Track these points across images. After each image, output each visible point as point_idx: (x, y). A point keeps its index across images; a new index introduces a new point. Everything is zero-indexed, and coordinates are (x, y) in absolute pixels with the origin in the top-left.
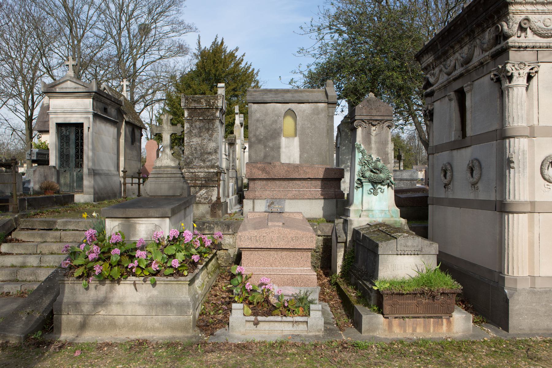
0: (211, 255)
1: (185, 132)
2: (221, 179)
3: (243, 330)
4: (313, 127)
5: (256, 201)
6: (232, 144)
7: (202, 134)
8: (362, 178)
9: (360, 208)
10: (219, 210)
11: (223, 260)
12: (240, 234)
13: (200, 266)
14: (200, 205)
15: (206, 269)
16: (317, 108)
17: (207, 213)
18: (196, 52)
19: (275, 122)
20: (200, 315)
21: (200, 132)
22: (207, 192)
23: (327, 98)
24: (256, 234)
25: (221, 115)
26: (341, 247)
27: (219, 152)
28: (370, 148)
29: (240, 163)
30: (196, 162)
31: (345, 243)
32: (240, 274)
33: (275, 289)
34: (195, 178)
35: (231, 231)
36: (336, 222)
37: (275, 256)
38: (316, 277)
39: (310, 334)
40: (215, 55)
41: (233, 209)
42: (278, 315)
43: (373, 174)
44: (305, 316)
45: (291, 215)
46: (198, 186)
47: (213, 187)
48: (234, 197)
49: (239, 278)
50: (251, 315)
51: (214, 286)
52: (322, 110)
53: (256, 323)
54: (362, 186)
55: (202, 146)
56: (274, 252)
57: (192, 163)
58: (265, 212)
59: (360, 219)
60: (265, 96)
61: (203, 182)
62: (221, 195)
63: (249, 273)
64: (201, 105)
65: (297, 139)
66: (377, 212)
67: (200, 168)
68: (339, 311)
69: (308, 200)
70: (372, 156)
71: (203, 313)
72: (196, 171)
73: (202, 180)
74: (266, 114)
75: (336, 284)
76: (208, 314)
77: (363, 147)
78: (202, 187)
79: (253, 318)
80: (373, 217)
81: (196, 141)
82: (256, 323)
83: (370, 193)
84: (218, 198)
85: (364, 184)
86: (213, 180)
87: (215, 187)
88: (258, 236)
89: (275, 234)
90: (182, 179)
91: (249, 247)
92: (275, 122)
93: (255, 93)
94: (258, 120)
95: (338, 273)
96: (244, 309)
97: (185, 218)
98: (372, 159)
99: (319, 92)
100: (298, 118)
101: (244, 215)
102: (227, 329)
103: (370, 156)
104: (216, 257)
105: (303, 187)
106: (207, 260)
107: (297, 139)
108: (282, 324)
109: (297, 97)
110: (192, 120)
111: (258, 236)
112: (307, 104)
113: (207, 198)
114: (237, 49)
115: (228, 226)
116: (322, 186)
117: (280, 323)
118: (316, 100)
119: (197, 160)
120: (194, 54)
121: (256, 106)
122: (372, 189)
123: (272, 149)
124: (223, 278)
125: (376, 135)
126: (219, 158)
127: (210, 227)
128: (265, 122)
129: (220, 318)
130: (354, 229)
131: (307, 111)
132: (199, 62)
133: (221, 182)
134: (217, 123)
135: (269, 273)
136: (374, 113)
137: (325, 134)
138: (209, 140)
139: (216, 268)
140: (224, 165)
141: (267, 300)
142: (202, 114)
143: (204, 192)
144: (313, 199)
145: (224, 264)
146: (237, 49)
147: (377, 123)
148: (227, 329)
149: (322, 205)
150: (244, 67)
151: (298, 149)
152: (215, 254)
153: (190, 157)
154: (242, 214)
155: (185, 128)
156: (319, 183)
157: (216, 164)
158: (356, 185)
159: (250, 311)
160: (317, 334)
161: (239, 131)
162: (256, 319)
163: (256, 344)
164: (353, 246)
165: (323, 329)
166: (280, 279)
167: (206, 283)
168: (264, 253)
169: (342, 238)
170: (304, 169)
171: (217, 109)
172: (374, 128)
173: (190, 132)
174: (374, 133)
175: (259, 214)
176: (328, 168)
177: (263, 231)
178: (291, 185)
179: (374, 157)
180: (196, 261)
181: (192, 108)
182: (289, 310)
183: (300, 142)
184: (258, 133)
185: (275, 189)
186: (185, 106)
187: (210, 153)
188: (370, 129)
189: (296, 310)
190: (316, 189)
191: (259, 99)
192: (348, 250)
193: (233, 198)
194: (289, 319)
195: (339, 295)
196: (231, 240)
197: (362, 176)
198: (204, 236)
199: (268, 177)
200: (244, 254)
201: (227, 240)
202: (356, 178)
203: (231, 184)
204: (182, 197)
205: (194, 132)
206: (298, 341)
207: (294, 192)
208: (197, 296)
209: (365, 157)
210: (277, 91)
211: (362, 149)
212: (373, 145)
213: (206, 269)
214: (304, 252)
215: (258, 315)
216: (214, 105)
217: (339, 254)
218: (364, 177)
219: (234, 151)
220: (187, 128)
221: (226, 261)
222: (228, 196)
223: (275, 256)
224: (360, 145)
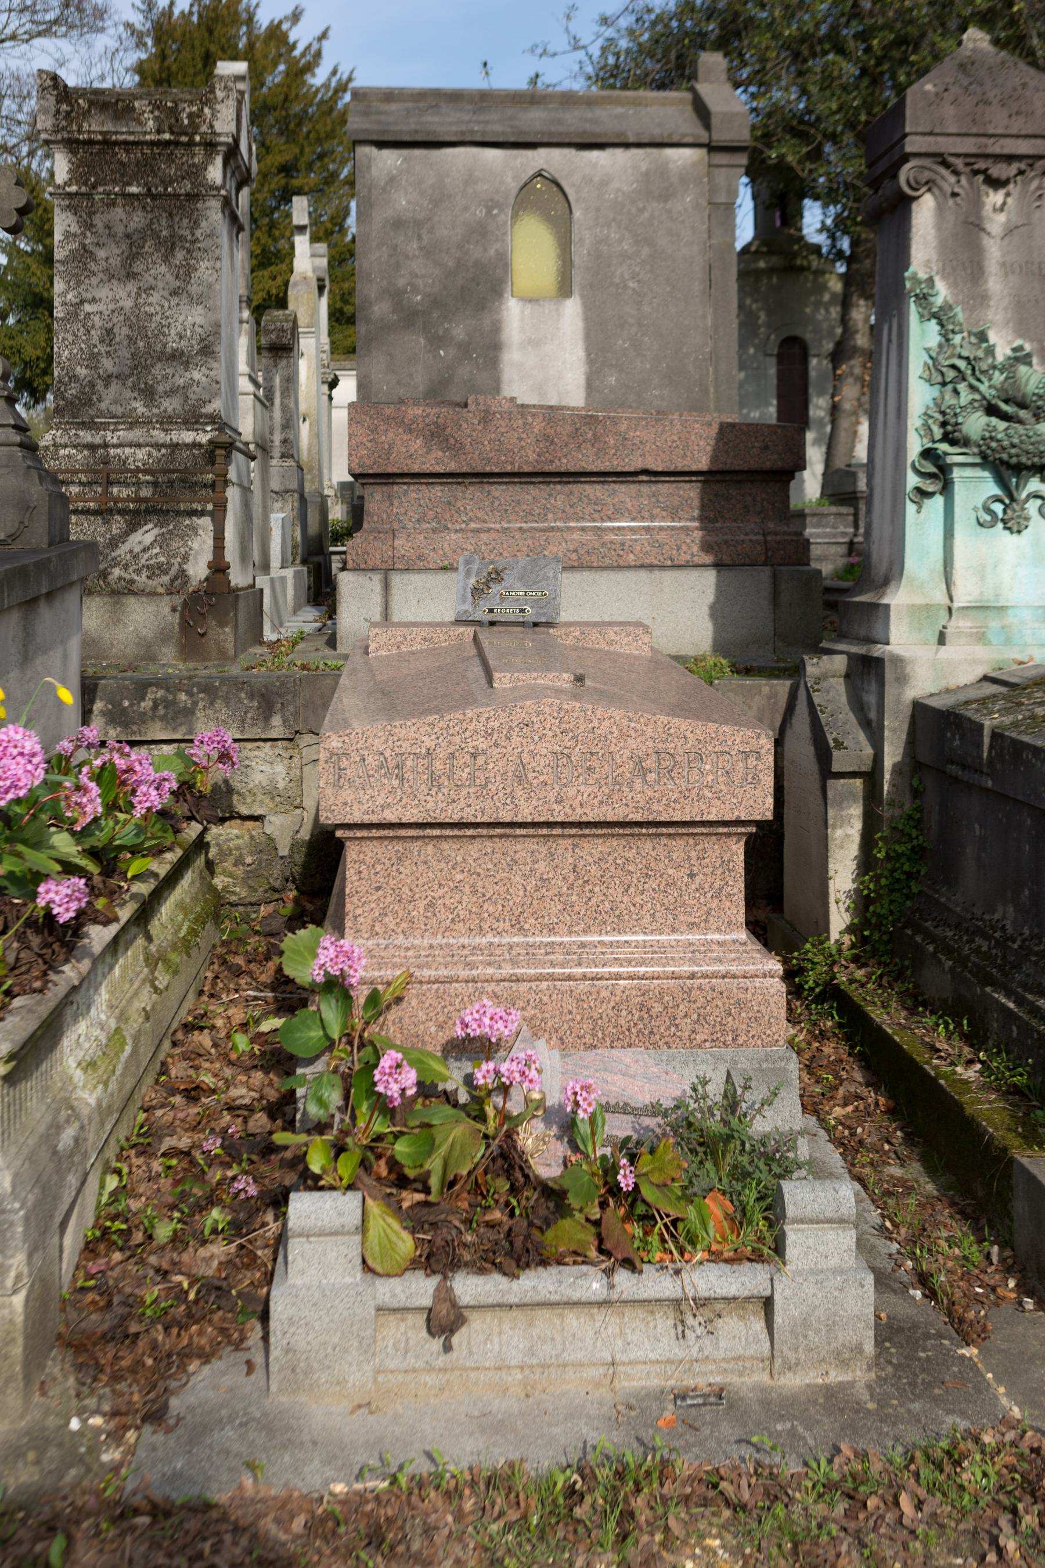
0: (172, 857)
1: (59, 254)
2: (232, 475)
3: (357, 1376)
4: (646, 251)
5: (396, 579)
6: (278, 349)
7: (138, 267)
8: (944, 447)
9: (940, 596)
10: (222, 624)
11: (240, 871)
12: (335, 743)
13: (98, 936)
14: (131, 602)
15: (140, 941)
16: (662, 170)
17: (164, 637)
18: (137, 19)
19: (481, 232)
20: (89, 1249)
21: (133, 256)
22: (161, 541)
23: (707, 126)
24: (428, 742)
25: (231, 184)
26: (843, 800)
27: (222, 350)
28: (978, 299)
29: (316, 436)
30: (109, 398)
31: (872, 777)
32: (336, 986)
33: (545, 1073)
34: (104, 472)
35: (277, 727)
36: (810, 669)
37: (542, 866)
38: (778, 987)
39: (793, 1381)
40: (211, 32)
41: (288, 618)
42: (579, 1257)
43: (1002, 425)
44: (757, 1257)
45: (594, 634)
46: (122, 512)
47: (194, 513)
48: (289, 573)
49: (329, 1011)
50: (414, 1264)
51: (188, 1028)
52: (684, 181)
53: (445, 1322)
54: (947, 488)
55: (137, 321)
56: (531, 845)
57: (89, 403)
58: (458, 622)
59: (945, 652)
60: (429, 119)
61: (146, 492)
62: (231, 554)
63: (388, 974)
64: (134, 127)
65: (572, 309)
66: (1026, 615)
67: (132, 426)
68: (896, 1171)
69: (643, 574)
70: (993, 337)
71: (105, 1231)
72: (111, 438)
73: (138, 484)
74: (440, 197)
75: (832, 994)
76: (138, 1237)
77: (942, 292)
78: (136, 518)
79: (421, 1288)
80: (1008, 641)
81: (108, 299)
82: (445, 1322)
83: (987, 521)
84: (219, 568)
85: (956, 473)
86: (189, 484)
87: (202, 513)
88: (442, 753)
89: (529, 742)
90: (19, 453)
91: (390, 816)
92: (481, 232)
93: (385, 107)
94: (398, 224)
95: (834, 935)
96: (363, 1228)
97: (26, 659)
98: (990, 351)
99: (664, 103)
100: (577, 214)
101: (341, 649)
102: (259, 1359)
103: (982, 337)
104: (200, 862)
105: (618, 513)
106: (143, 888)
107: (572, 309)
108: (610, 1322)
109: (574, 121)
110: (89, 196)
111: (442, 753)
112: (619, 152)
113: (158, 570)
114: (296, 17)
115: (267, 701)
116: (703, 507)
117: (599, 1315)
118: (657, 133)
119: (114, 387)
120: (128, 25)
121: (389, 160)
122: (999, 500)
123: (465, 349)
124: (238, 972)
125: (1010, 231)
126: (223, 379)
127: (168, 704)
128: (431, 231)
129: (210, 1271)
130: (918, 707)
131: (615, 185)
132: (149, 60)
133: (233, 494)
134: (214, 215)
135: (507, 970)
136: (998, 120)
137: (697, 287)
138: (175, 293)
139: (200, 920)
140: (247, 425)
141: (508, 1160)
142: (145, 168)
143: (149, 538)
144: (662, 567)
145: (242, 892)
146: (296, 17)
147: (1013, 169)
148: (259, 1359)
149: (710, 597)
150: (326, 86)
151: (581, 353)
152: (200, 844)
153: (81, 371)
154: (332, 642)
155: (58, 236)
156: (691, 493)
157: (209, 409)
158: (912, 480)
159: (406, 1244)
160: (836, 1376)
161: (311, 312)
162: (445, 1295)
163: (452, 1495)
164: (916, 794)
165: (869, 1348)
166: (569, 1004)
167: (136, 1021)
168: (474, 849)
169: (853, 749)
170: (623, 427)
171: (210, 146)
172: (996, 198)
173: (83, 256)
174: (996, 223)
175: (425, 632)
176: (732, 425)
177: (474, 723)
178: (560, 501)
179: (1002, 344)
180: (64, 914)
181: (90, 142)
182: (648, 1219)
183: (587, 319)
184: (401, 282)
185: (487, 522)
186: (57, 129)
187: (179, 358)
188: (977, 204)
189: (691, 1213)
190: (673, 520)
191: (405, 129)
192: (886, 812)
193: (283, 580)
194: (655, 1283)
195: (866, 1062)
196: (280, 769)
197: (946, 438)
198: (135, 754)
199: (452, 467)
200: (360, 865)
201: (263, 769)
202: (915, 446)
203: (277, 518)
204: (16, 547)
205: (101, 253)
206: (719, 1448)
207: (576, 536)
208: (67, 1136)
209: (957, 339)
210: (484, 99)
211: (939, 301)
212: (995, 284)
213: (140, 941)
214: (706, 843)
215: (455, 1265)
216: (194, 127)
217: (837, 834)
218: (953, 443)
219: (291, 382)
220: (68, 236)
221: (252, 875)
222: (266, 567)
223: (542, 866)
224: (930, 281)
